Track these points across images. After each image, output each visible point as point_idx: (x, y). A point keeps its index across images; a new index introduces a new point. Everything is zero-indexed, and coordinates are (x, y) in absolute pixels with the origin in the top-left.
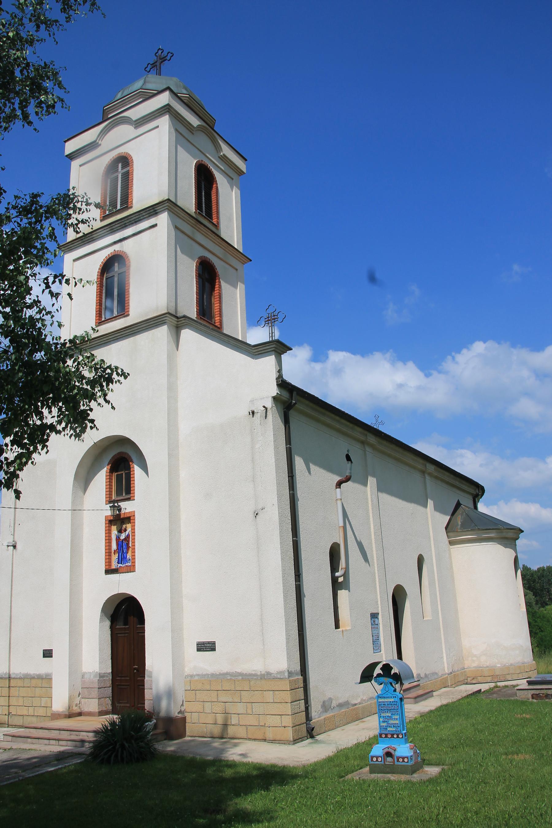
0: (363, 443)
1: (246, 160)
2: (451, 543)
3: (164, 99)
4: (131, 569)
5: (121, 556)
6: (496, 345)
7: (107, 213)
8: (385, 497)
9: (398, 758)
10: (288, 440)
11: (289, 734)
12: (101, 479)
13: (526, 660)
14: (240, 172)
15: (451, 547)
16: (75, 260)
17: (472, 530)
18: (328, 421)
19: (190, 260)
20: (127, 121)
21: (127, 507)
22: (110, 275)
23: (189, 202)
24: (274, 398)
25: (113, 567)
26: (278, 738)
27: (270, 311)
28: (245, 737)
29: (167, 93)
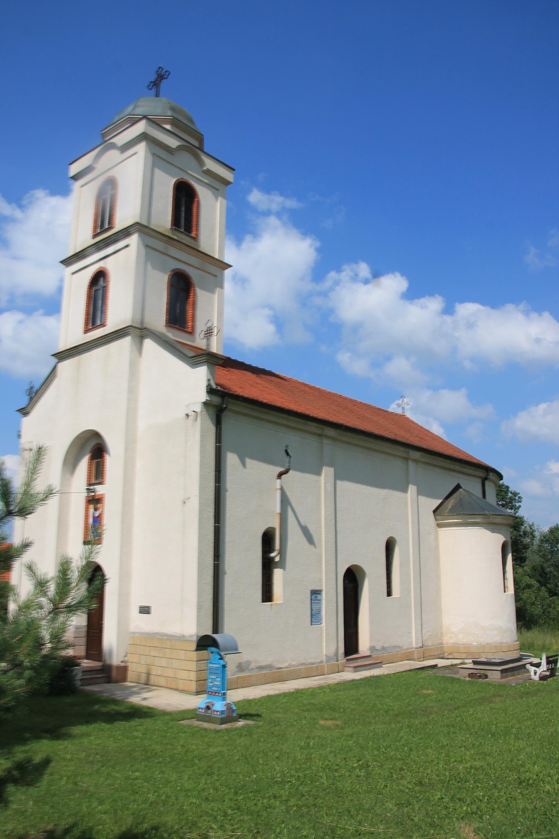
0: (320, 435)
1: (234, 170)
2: (439, 526)
3: (141, 127)
5: (93, 534)
7: (99, 231)
8: (344, 486)
9: (214, 711)
10: (219, 439)
11: (193, 687)
12: (84, 464)
13: (504, 641)
14: (226, 183)
15: (439, 529)
17: (457, 515)
18: (272, 418)
20: (113, 146)
21: (100, 490)
23: (163, 218)
24: (206, 404)
26: (186, 689)
27: (208, 326)
28: (166, 686)
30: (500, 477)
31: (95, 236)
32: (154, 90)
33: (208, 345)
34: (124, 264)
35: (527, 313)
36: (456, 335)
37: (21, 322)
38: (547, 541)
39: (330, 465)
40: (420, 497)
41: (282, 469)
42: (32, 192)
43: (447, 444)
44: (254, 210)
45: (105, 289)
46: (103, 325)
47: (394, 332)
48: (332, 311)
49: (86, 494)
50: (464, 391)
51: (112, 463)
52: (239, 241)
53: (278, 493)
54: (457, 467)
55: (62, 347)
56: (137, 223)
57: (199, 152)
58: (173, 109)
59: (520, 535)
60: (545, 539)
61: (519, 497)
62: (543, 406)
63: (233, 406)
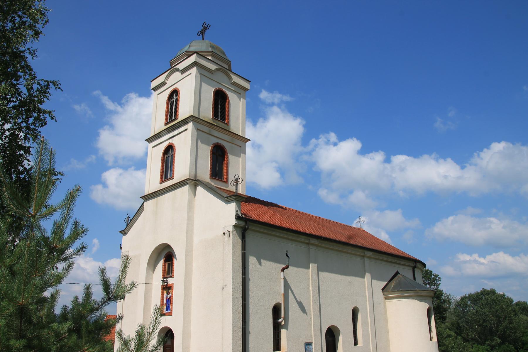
0: (308, 244)
2: (386, 298)
3: (193, 58)
4: (170, 314)
5: (166, 307)
6: (511, 145)
8: (324, 275)
10: (244, 248)
14: (246, 90)
16: (153, 147)
19: (207, 146)
20: (177, 70)
21: (170, 281)
22: (168, 156)
23: (207, 112)
24: (235, 226)
25: (164, 313)
27: (236, 177)
29: (195, 55)
30: (424, 265)
31: (166, 124)
32: (201, 36)
33: (236, 189)
34: (184, 141)
35: (437, 160)
36: (394, 175)
37: (121, 175)
38: (460, 306)
39: (315, 263)
40: (373, 281)
41: (284, 266)
42: (127, 95)
43: (390, 246)
44: (263, 103)
45: (173, 156)
46: (172, 178)
47: (355, 176)
48: (314, 164)
49: (161, 284)
50: (400, 210)
51: (178, 264)
52: (255, 122)
53: (282, 281)
54: (396, 261)
55: (146, 193)
56: (192, 116)
57: (228, 71)
58: (212, 47)
59: (442, 303)
60: (458, 304)
61: (439, 278)
62: (451, 218)
63: (252, 227)
